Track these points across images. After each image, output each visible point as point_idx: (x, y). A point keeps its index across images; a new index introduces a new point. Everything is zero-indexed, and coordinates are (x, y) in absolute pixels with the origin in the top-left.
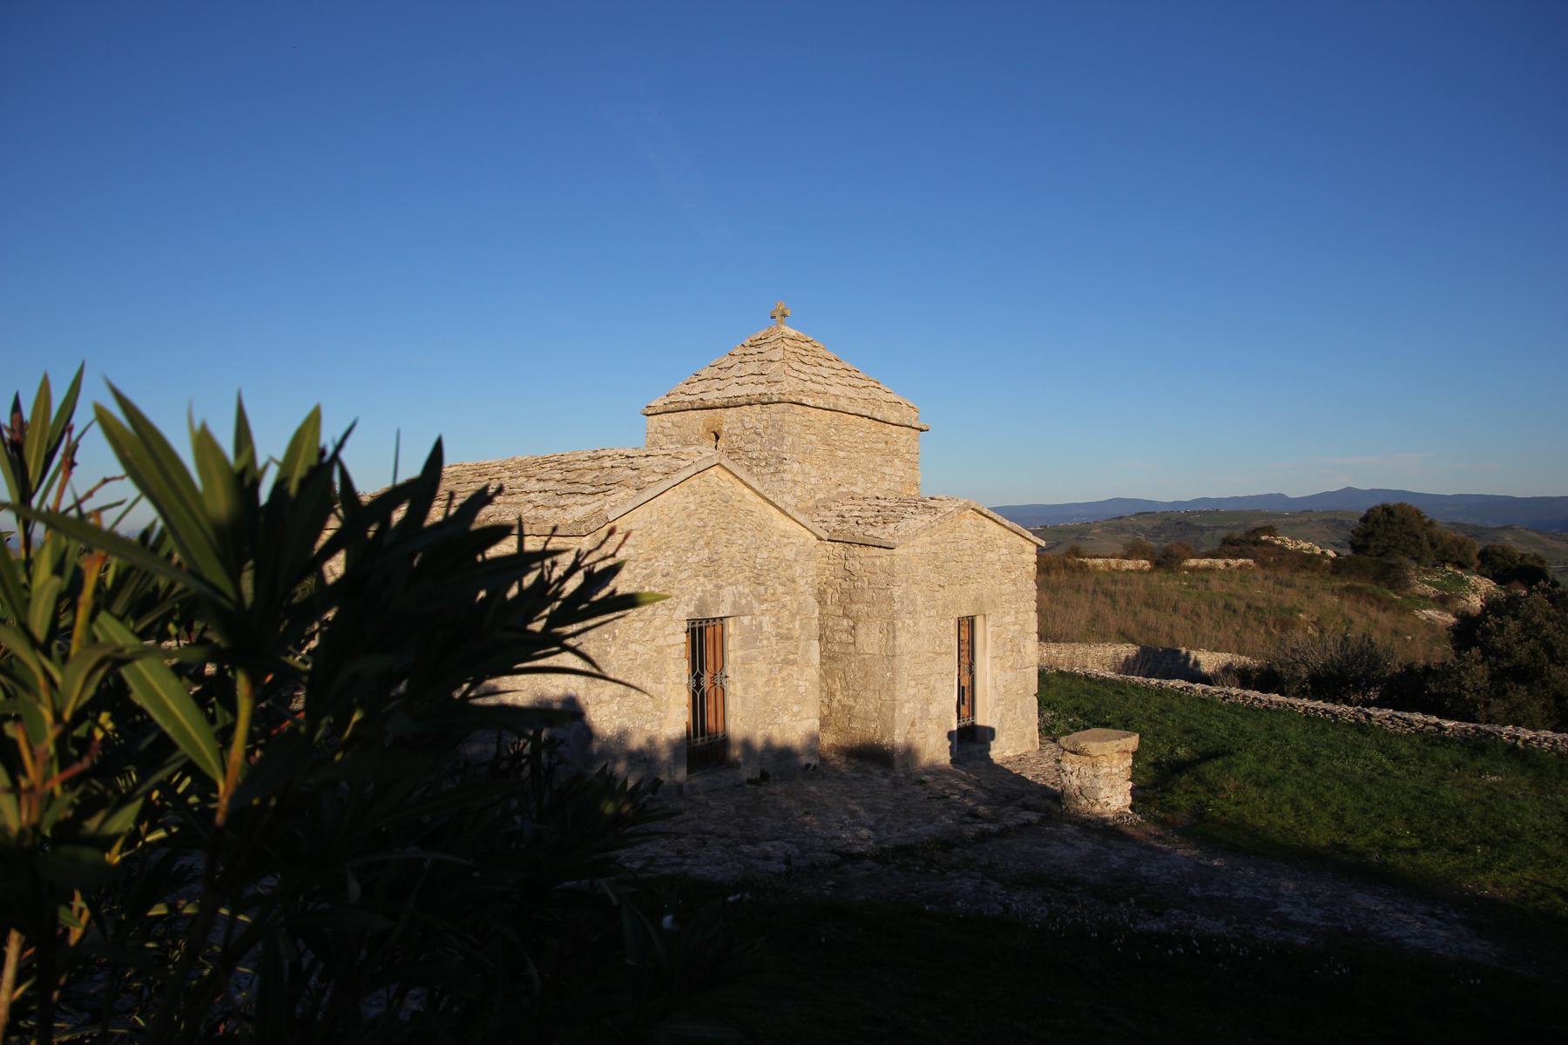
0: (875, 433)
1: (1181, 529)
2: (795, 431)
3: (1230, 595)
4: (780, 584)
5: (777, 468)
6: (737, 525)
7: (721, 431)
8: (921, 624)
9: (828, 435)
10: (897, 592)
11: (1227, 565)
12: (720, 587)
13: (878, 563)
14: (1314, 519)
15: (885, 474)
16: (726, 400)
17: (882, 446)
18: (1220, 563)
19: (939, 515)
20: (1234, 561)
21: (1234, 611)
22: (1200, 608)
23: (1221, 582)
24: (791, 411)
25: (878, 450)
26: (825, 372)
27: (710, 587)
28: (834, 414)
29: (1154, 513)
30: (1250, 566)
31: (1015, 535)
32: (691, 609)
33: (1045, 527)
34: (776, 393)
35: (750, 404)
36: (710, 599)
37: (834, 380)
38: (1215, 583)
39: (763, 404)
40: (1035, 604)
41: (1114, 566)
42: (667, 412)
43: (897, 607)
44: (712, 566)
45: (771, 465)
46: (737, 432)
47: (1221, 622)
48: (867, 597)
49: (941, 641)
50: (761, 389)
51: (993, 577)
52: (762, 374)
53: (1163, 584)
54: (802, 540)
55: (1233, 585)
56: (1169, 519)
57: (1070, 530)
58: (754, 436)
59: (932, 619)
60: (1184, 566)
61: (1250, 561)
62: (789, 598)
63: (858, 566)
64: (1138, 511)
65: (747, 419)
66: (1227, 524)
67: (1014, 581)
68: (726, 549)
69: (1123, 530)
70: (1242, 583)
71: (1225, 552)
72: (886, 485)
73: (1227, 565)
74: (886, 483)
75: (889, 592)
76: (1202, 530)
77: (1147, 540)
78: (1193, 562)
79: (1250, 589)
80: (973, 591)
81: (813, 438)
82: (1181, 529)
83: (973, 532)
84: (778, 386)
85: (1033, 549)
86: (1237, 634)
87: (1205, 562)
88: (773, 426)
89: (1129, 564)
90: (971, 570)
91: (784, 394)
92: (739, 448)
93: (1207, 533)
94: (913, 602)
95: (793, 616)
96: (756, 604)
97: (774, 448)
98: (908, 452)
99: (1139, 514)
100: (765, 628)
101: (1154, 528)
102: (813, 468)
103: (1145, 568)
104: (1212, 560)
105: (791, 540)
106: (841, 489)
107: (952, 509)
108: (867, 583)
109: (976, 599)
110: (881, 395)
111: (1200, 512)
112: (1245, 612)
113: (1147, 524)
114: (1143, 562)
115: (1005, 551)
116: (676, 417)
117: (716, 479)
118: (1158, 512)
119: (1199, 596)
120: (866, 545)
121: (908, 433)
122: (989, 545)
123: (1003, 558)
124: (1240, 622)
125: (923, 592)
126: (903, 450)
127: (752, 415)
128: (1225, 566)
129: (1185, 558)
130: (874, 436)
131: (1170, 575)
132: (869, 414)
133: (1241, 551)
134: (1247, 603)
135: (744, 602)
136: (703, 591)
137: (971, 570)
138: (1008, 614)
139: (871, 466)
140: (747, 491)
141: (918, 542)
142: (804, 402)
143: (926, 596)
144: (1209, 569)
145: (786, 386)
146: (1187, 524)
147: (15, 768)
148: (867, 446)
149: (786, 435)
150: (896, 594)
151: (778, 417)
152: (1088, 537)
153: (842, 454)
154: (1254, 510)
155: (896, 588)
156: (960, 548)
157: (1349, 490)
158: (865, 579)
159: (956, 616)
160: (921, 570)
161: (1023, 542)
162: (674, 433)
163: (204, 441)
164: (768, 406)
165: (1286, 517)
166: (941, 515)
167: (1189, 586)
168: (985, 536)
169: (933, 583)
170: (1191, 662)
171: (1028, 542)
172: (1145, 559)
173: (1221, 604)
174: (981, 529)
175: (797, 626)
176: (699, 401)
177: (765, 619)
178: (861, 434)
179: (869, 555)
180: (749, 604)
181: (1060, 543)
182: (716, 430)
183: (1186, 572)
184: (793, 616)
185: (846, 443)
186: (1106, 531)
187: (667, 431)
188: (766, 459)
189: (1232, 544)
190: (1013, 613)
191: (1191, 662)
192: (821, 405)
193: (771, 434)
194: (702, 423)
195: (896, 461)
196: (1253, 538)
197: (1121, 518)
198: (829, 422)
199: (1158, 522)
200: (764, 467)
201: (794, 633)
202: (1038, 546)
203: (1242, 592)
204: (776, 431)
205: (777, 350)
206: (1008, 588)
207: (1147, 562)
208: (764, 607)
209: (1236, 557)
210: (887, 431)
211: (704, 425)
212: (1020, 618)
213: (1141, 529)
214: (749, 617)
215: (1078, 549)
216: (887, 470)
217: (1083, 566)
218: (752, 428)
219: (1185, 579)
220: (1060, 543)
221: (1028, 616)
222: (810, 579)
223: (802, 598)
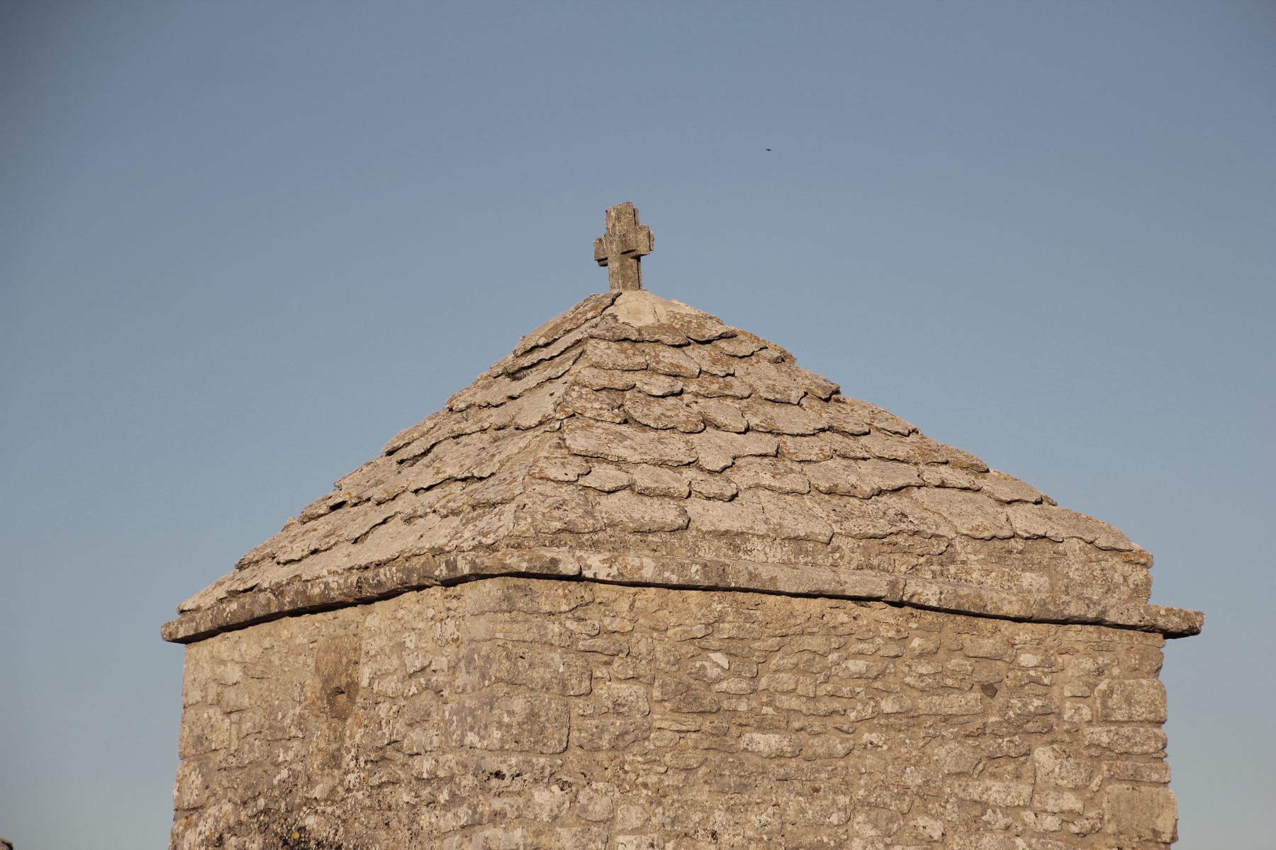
2: (539, 674)
9: (700, 675)
15: (984, 805)
16: (354, 579)
25: (947, 719)
28: (718, 603)
98: (1106, 720)
116: (248, 643)
121: (1100, 648)
139: (913, 779)
153: (765, 742)
162: (246, 701)
187: (231, 696)
192: (648, 574)
198: (698, 631)
200: (447, 806)
204: (475, 677)
210: (987, 646)
211: (317, 669)
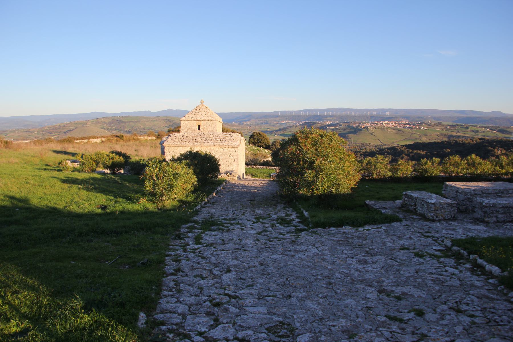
1: (118, 123)
14: (160, 119)
33: (70, 122)
41: (146, 139)
57: (80, 123)
66: (133, 121)
69: (99, 123)
76: (125, 123)
82: (118, 123)
89: (150, 138)
101: (109, 122)
110: (409, 130)
111: (124, 117)
113: (107, 121)
116: (189, 122)
127: (209, 123)
146: (120, 121)
147: (454, 340)
152: (87, 126)
157: (170, 110)
163: (355, 185)
165: (152, 118)
181: (77, 128)
182: (200, 124)
186: (93, 123)
199: (110, 120)
213: (105, 123)
217: (138, 139)
220: (77, 128)
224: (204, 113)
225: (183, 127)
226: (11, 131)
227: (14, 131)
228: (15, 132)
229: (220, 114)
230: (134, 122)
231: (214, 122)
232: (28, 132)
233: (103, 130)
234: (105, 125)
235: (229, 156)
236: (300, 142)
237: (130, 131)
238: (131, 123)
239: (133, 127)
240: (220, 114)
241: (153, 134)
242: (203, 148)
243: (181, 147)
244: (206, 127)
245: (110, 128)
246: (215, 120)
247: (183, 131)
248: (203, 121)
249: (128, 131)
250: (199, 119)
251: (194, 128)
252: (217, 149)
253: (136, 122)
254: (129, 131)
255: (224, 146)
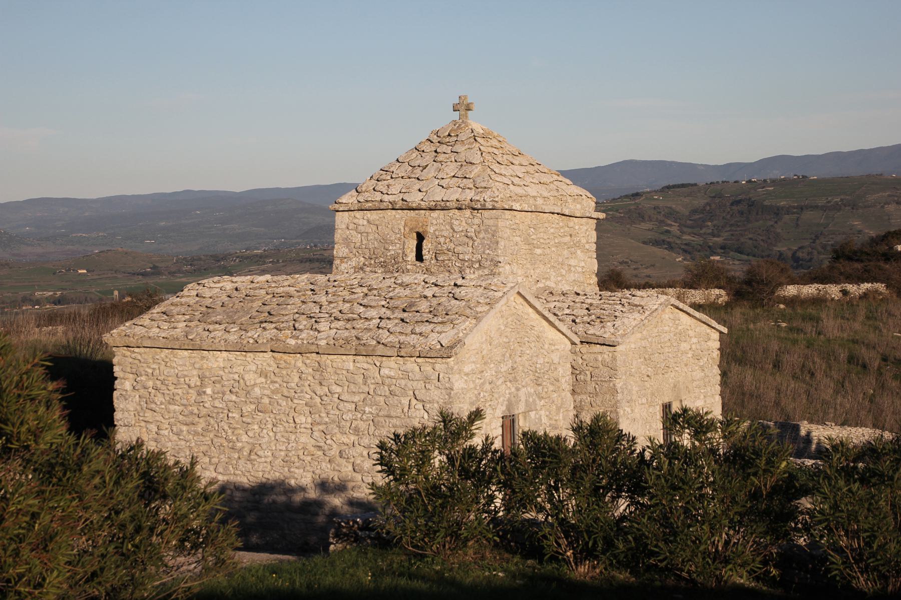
0: (562, 227)
1: (741, 213)
2: (506, 235)
3: (855, 342)
4: (551, 384)
5: (492, 271)
6: (526, 339)
7: (426, 232)
8: (636, 411)
10: (619, 384)
11: (845, 292)
12: (518, 389)
13: (600, 359)
16: (434, 204)
17: (567, 239)
18: (834, 291)
19: (647, 313)
20: (855, 287)
21: (864, 366)
22: (814, 363)
23: (839, 321)
24: (503, 216)
25: (565, 244)
26: (520, 171)
27: (513, 390)
29: (695, 185)
30: (881, 294)
31: (702, 324)
32: (504, 408)
34: (488, 200)
35: (460, 209)
36: (513, 399)
37: (528, 179)
38: (831, 325)
39: (474, 209)
40: (719, 387)
42: (362, 210)
43: (620, 397)
44: (512, 376)
45: (485, 268)
46: (445, 233)
47: (847, 384)
48: (590, 388)
49: (650, 426)
50: (470, 195)
51: (686, 365)
52: (465, 178)
53: (751, 326)
54: (563, 346)
55: (857, 326)
56: (719, 195)
58: (467, 240)
59: (643, 406)
60: (779, 296)
61: (881, 287)
62: (556, 395)
63: (580, 361)
64: (665, 183)
65: (456, 223)
66: (821, 202)
67: (702, 369)
68: (520, 359)
69: (641, 217)
70: (871, 322)
71: (841, 274)
72: (572, 277)
73: (845, 292)
74: (572, 275)
75: (611, 384)
76: (777, 212)
77: (683, 232)
78: (791, 290)
79: (885, 331)
80: (672, 378)
81: (518, 239)
82: (741, 213)
83: (671, 325)
84: (489, 193)
85: (716, 336)
86: (871, 401)
87: (810, 290)
88: (486, 231)
90: (670, 360)
91: (497, 202)
92: (449, 250)
93: (787, 217)
94: (630, 391)
95: (558, 409)
96: (538, 402)
97: (487, 251)
98: (587, 242)
99: (668, 187)
100: (543, 421)
101: (694, 211)
102: (518, 268)
103: (720, 301)
104: (821, 286)
105: (556, 347)
106: (540, 285)
107: (656, 307)
108: (589, 376)
109: (675, 386)
111: (774, 182)
112: (879, 368)
113: (681, 205)
114: (717, 291)
115: (695, 340)
116: (373, 216)
117: (514, 304)
118: (701, 183)
119: (809, 345)
120: (587, 343)
121: (587, 224)
122: (682, 336)
123: (694, 347)
124: (874, 382)
125: (637, 382)
126: (584, 241)
127: (462, 220)
128: (841, 295)
129: (781, 284)
130: (562, 231)
131: (758, 311)
132: (559, 211)
133: (868, 271)
134: (882, 355)
135: (531, 400)
136: (509, 393)
137: (670, 360)
138: (699, 398)
140: (531, 310)
141: (633, 338)
142: (514, 208)
143: (639, 386)
144: (818, 301)
145: (497, 193)
146: (752, 204)
148: (557, 241)
149: (500, 239)
150: (619, 386)
151: (491, 222)
153: (538, 251)
154: (869, 176)
155: (618, 381)
156: (662, 340)
158: (587, 372)
159: (660, 403)
160: (635, 363)
161: (709, 330)
164: (480, 211)
166: (648, 313)
167: (791, 329)
168: (680, 328)
169: (643, 375)
170: (814, 446)
171: (713, 330)
172: (720, 288)
173: (843, 355)
174: (677, 322)
175: (561, 418)
176: (401, 202)
177: (543, 413)
178: (552, 230)
179: (591, 351)
180: (534, 401)
182: (421, 230)
183: (782, 306)
184: (558, 409)
185: (542, 241)
188: (479, 262)
189: (850, 259)
190: (702, 397)
191: (814, 446)
192: (526, 209)
193: (484, 238)
194: (403, 223)
195: (579, 252)
196: (883, 248)
197: (637, 195)
199: (699, 202)
201: (558, 423)
202: (721, 333)
203: (872, 337)
204: (490, 236)
205: (472, 151)
206: (698, 374)
207: (723, 292)
208: (542, 402)
209: (859, 280)
212: (708, 402)
213: (672, 214)
214: (534, 412)
215: (618, 275)
216: (573, 262)
218: (462, 231)
219: (783, 316)
221: (714, 399)
222: (567, 378)
223: (563, 394)
224: (451, 169)
225: (347, 241)
226: (247, 258)
227: (261, 256)
228: (264, 263)
229: (577, 176)
230: (824, 208)
231: (486, 213)
232: (318, 260)
233: (660, 252)
234: (675, 229)
235: (405, 402)
236: (68, 342)
237: (800, 254)
238: (807, 215)
239: (817, 237)
240: (577, 176)
241: (717, 278)
242: (285, 357)
243: (186, 353)
244: (452, 246)
245: (697, 240)
246: (489, 205)
247: (343, 266)
248: (435, 214)
249: (790, 254)
250: (415, 198)
251: (393, 249)
252: (348, 363)
253: (837, 207)
254: (796, 259)
255: (380, 350)
